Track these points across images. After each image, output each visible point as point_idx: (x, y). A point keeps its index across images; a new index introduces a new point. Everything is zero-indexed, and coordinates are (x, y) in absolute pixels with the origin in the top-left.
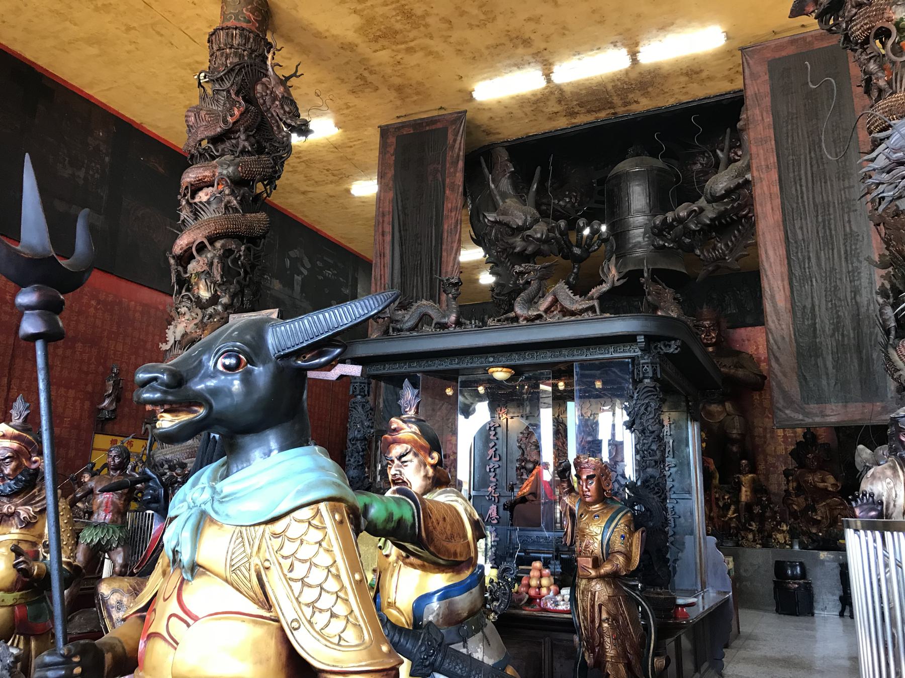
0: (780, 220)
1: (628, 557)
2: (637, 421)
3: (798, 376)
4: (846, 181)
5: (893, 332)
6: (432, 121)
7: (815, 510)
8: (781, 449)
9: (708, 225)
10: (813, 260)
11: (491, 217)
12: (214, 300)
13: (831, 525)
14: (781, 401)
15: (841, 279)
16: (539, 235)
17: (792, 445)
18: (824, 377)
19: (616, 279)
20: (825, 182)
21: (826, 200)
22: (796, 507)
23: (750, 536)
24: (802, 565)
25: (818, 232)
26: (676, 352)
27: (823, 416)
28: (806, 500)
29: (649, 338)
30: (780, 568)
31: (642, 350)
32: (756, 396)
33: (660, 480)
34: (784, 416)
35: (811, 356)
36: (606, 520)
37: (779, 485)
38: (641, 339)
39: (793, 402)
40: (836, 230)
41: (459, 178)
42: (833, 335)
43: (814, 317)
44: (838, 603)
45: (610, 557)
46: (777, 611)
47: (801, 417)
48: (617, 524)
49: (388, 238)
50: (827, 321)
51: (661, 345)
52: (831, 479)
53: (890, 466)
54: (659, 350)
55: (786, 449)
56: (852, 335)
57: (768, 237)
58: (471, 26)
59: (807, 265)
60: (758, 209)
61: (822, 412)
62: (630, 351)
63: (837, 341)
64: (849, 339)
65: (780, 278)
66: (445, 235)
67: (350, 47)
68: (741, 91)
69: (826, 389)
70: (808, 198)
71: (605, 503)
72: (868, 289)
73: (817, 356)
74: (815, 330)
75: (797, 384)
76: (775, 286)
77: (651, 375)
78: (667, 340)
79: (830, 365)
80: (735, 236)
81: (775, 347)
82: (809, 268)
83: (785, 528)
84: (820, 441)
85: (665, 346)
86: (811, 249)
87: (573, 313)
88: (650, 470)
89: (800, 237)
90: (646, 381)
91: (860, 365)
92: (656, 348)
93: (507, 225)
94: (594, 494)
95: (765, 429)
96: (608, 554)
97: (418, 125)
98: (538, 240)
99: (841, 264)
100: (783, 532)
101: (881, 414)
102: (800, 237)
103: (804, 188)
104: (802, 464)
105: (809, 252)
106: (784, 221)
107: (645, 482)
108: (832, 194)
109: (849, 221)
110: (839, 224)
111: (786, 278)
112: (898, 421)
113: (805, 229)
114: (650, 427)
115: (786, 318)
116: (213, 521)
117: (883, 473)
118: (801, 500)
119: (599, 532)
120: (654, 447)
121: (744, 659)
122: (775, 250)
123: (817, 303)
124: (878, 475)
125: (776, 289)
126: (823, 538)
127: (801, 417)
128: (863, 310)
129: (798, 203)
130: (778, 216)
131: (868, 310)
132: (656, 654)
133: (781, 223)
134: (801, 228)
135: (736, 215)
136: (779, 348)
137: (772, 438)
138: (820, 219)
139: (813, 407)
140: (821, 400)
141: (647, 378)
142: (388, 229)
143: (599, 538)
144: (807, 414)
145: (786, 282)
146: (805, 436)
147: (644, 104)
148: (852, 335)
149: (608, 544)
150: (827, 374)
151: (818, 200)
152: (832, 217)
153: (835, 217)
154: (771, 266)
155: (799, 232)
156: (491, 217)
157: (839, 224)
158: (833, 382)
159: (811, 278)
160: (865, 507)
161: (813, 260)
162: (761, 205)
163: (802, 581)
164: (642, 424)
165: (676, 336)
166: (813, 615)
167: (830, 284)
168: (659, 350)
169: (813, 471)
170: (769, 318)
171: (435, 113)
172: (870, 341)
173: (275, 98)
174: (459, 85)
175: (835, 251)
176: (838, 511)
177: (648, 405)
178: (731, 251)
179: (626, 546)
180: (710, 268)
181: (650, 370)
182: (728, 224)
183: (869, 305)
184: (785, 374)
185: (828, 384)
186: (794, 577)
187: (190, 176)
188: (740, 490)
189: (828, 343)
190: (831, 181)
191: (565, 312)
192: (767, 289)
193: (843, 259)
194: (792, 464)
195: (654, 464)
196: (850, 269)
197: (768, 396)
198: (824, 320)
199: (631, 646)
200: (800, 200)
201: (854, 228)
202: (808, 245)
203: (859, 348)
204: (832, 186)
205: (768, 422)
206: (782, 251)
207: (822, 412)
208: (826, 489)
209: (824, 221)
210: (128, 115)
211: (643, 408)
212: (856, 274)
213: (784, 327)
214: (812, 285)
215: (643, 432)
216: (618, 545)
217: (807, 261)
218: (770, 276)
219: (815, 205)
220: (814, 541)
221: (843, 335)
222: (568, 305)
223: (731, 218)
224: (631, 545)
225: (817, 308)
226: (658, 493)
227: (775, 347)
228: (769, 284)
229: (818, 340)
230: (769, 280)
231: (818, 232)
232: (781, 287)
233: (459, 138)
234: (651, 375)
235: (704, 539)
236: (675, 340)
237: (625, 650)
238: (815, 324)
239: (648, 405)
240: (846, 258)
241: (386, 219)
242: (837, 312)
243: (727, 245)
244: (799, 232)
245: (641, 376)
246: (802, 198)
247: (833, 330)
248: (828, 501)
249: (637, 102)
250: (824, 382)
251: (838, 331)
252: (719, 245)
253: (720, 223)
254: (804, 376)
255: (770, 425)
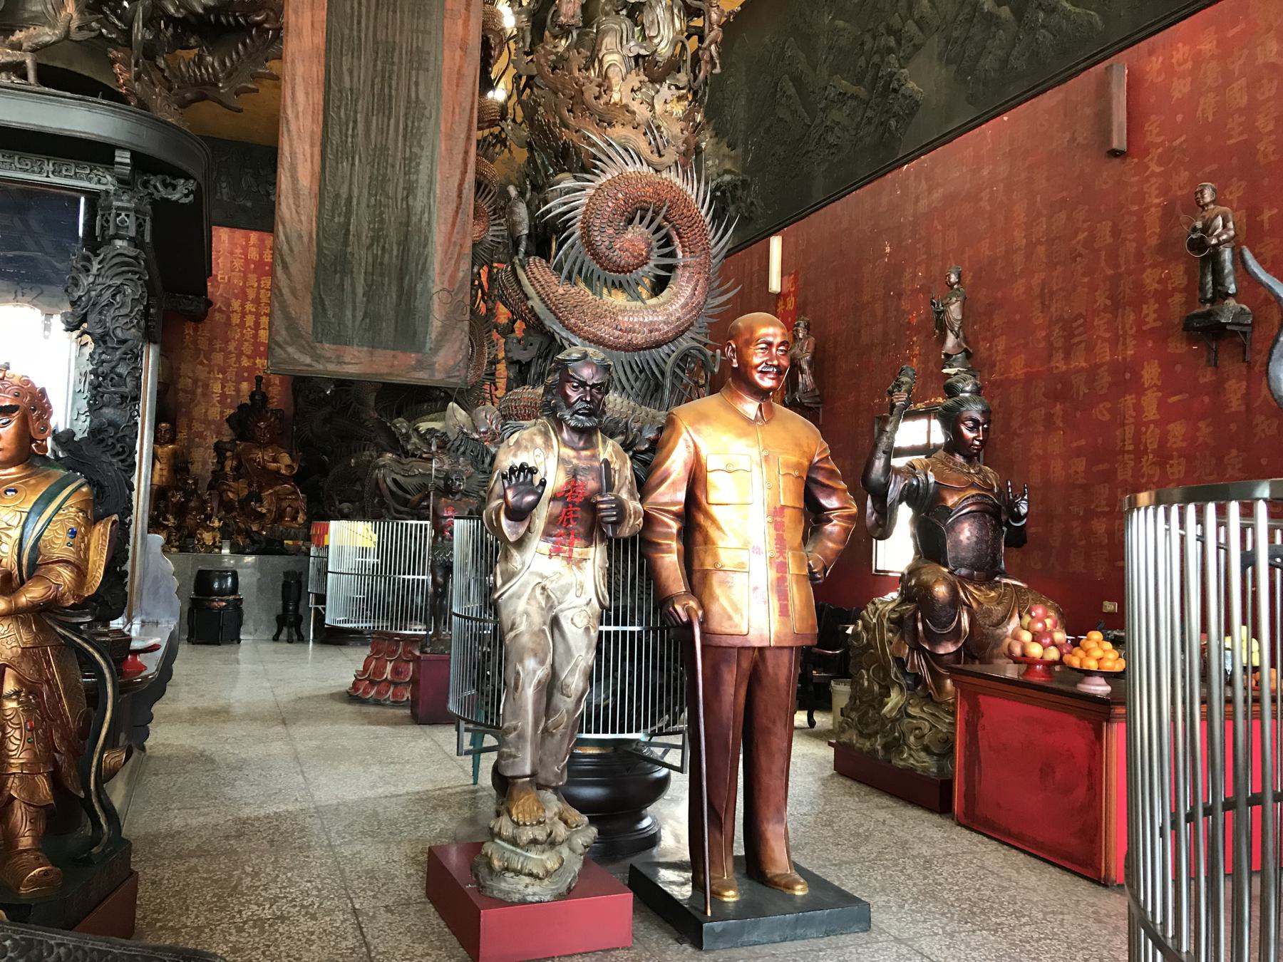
0: (322, 47)
1: (80, 570)
2: (93, 317)
3: (314, 298)
4: (421, 21)
5: (524, 243)
7: (260, 500)
8: (215, 413)
9: (197, 15)
10: (361, 127)
13: (274, 521)
14: (284, 332)
15: (393, 166)
17: (231, 407)
18: (350, 306)
19: (74, 25)
20: (394, 12)
21: (391, 40)
22: (231, 495)
25: (373, 85)
26: (186, 200)
27: (339, 363)
28: (250, 485)
29: (141, 162)
31: (120, 181)
32: (189, 330)
33: (127, 432)
34: (284, 355)
35: (335, 272)
36: (35, 498)
37: (205, 463)
38: (123, 157)
39: (300, 336)
40: (397, 90)
42: (370, 247)
43: (348, 214)
44: (275, 623)
45: (42, 571)
47: (308, 360)
48: (59, 508)
50: (366, 225)
51: (156, 181)
52: (286, 459)
53: (540, 431)
54: (152, 190)
55: (222, 412)
56: (395, 253)
57: (300, 69)
59: (350, 132)
60: (290, 18)
61: (338, 357)
62: (90, 180)
63: (375, 257)
64: (391, 258)
65: (308, 140)
69: (349, 324)
70: (367, 28)
71: (30, 466)
72: (426, 190)
73: (344, 273)
74: (348, 231)
75: (310, 310)
76: (299, 150)
77: (132, 233)
78: (172, 173)
79: (360, 291)
80: (237, 53)
81: (285, 247)
82: (353, 136)
83: (216, 524)
84: (270, 406)
85: (166, 185)
86: (360, 107)
88: (108, 412)
89: (347, 85)
90: (119, 243)
91: (399, 297)
92: (145, 184)
94: (12, 447)
95: (196, 381)
96: (33, 566)
99: (396, 141)
100: (213, 529)
101: (414, 369)
102: (347, 85)
103: (364, 9)
104: (241, 436)
105: (356, 112)
106: (328, 50)
107: (95, 432)
108: (401, 32)
109: (417, 84)
110: (403, 82)
111: (318, 144)
112: (566, 367)
113: (355, 74)
114: (119, 332)
115: (309, 206)
117: (532, 441)
118: (242, 484)
119: (15, 523)
120: (122, 369)
121: (165, 717)
122: (307, 93)
123: (356, 194)
124: (524, 443)
125: (300, 156)
126: (266, 538)
127: (308, 360)
128: (414, 219)
129: (351, 30)
130: (320, 40)
131: (420, 220)
132: (111, 743)
133: (323, 53)
134: (351, 73)
135: (245, 17)
136: (291, 249)
137: (204, 395)
138: (379, 67)
139: (328, 348)
140: (340, 339)
141: (122, 238)
143: (16, 534)
144: (318, 358)
145: (317, 150)
146: (252, 396)
148: (395, 253)
149: (35, 547)
150: (354, 302)
151: (381, 36)
152: (395, 68)
153: (399, 69)
154: (297, 117)
155: (347, 79)
157: (403, 82)
158: (360, 314)
159: (354, 153)
160: (522, 488)
161: (361, 127)
162: (296, 12)
163: (231, 597)
164: (102, 323)
165: (191, 171)
166: (239, 641)
167: (378, 170)
168: (152, 190)
169: (263, 447)
170: (283, 198)
172: (417, 265)
175: (392, 121)
176: (288, 502)
177: (118, 290)
178: (229, 75)
179: (78, 552)
180: (188, 95)
181: (131, 223)
182: (228, 29)
183: (423, 212)
184: (293, 291)
185: (354, 316)
186: (221, 593)
189: (361, 255)
190: (402, 12)
192: (287, 154)
193: (400, 137)
194: (227, 435)
195: (118, 400)
196: (408, 155)
197: (206, 333)
198: (361, 223)
199: (62, 739)
200: (355, 27)
201: (421, 96)
202: (357, 101)
203: (402, 273)
204: (402, 21)
205: (201, 372)
206: (318, 98)
207: (338, 357)
208: (277, 472)
209: (383, 70)
211: (108, 294)
212: (413, 164)
213: (304, 218)
214: (353, 164)
215: (100, 340)
216: (59, 546)
217: (351, 125)
218: (294, 133)
219: (376, 42)
220: (254, 542)
221: (383, 249)
223: (236, 19)
224: (87, 548)
225: (355, 201)
226: (118, 454)
227: (285, 247)
228: (291, 146)
229: (349, 249)
230: (291, 140)
231: (373, 85)
232: (308, 156)
234: (132, 233)
235: (143, 538)
236: (187, 177)
237: (50, 748)
238: (349, 224)
239: (118, 290)
240: (405, 136)
242: (381, 213)
243: (223, 63)
244: (347, 79)
245: (112, 231)
246: (359, 23)
247: (372, 239)
248: (278, 488)
250: (349, 313)
251: (378, 242)
252: (209, 59)
253: (218, 19)
254: (322, 299)
255: (203, 376)
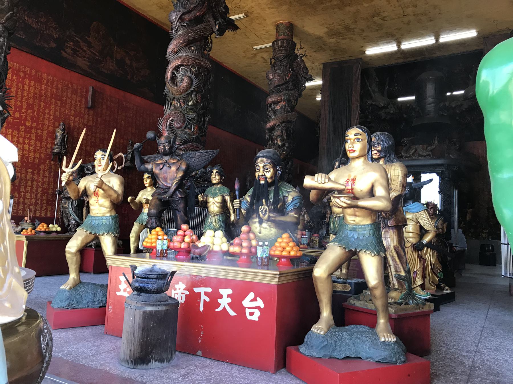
6: (346, 62)
11: (369, 102)
12: (283, 145)
16: (392, 112)
22: (491, 223)
23: (470, 235)
24: (492, 246)
30: (483, 247)
41: (359, 86)
46: (480, 264)
49: (327, 112)
58: (372, 32)
66: (352, 111)
67: (320, 38)
68: (482, 49)
87: (422, 156)
93: (377, 106)
97: (340, 63)
98: (392, 114)
116: (407, 212)
142: (327, 108)
147: (438, 54)
156: (369, 102)
166: (495, 265)
171: (348, 58)
173: (300, 67)
174: (361, 49)
186: (488, 251)
187: (270, 100)
188: (466, 216)
191: (420, 155)
210: (218, 60)
216: (440, 226)
222: (421, 153)
233: (358, 70)
241: (326, 104)
249: (435, 54)
